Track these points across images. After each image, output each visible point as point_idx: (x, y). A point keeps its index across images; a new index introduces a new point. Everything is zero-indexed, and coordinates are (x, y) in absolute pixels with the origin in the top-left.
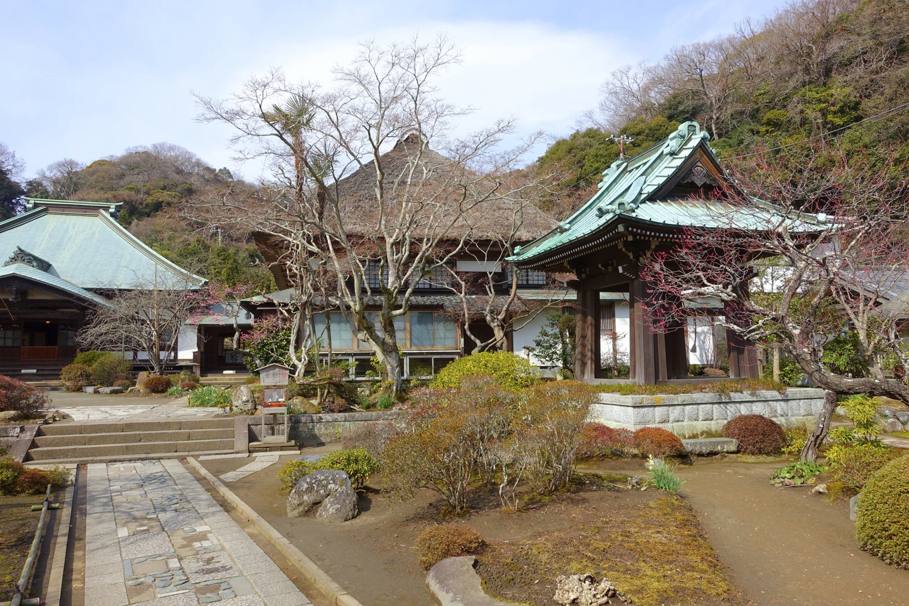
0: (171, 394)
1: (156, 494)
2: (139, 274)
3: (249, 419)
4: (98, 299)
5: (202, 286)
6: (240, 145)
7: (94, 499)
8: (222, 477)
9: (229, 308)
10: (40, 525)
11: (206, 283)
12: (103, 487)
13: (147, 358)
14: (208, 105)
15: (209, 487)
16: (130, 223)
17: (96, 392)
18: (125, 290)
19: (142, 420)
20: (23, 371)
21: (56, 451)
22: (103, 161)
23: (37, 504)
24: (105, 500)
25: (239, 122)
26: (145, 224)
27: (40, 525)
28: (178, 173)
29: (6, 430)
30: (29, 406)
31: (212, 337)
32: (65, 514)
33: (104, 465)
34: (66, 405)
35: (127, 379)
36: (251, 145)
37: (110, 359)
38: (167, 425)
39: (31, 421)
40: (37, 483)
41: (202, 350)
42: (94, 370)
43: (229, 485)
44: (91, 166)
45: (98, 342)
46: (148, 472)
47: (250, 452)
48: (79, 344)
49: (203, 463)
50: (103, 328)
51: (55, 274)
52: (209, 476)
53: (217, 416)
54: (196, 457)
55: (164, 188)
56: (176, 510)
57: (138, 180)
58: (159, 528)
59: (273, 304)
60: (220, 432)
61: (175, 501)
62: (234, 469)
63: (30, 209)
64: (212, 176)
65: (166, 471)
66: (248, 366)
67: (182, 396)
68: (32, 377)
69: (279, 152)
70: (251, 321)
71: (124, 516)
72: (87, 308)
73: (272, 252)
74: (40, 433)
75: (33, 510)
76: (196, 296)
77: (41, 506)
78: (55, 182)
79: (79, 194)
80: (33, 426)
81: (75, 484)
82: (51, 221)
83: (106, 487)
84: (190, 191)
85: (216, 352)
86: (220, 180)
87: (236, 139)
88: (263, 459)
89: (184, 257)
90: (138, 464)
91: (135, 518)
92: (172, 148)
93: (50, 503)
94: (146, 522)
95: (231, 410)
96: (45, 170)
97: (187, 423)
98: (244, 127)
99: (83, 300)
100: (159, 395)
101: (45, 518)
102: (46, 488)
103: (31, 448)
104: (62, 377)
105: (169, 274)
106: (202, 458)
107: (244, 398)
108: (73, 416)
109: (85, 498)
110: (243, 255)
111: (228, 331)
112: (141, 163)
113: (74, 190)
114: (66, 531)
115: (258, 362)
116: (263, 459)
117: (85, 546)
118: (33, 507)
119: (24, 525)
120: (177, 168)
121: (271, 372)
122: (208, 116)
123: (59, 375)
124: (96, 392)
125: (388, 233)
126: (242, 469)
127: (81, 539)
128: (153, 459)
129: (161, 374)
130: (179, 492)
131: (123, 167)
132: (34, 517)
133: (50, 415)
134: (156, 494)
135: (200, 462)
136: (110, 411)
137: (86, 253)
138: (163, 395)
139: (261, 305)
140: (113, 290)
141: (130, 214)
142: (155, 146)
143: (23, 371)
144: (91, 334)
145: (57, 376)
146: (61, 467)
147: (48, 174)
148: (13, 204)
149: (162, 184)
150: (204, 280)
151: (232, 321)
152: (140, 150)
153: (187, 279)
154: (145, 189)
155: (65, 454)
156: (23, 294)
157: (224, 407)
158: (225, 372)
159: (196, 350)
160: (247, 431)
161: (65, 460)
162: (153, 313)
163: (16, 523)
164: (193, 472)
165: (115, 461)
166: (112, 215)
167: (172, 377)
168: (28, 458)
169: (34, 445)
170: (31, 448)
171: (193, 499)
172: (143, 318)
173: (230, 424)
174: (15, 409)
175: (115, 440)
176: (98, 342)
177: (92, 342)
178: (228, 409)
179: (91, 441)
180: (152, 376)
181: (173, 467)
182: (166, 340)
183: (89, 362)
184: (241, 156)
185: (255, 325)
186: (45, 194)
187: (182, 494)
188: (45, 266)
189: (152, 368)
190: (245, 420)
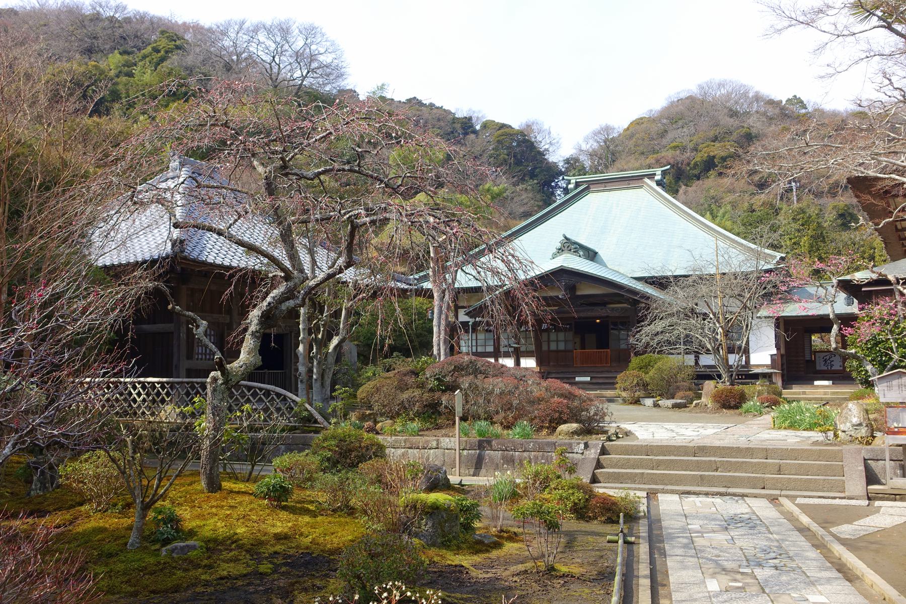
0: (747, 411)
1: (748, 542)
2: (696, 253)
3: (866, 451)
4: (650, 290)
5: (778, 263)
6: (827, 56)
7: (672, 537)
8: (834, 530)
9: (821, 291)
10: (619, 560)
11: (782, 259)
12: (680, 524)
13: (713, 363)
14: (778, 11)
15: (816, 542)
16: (677, 191)
17: (656, 405)
18: (681, 276)
19: (717, 443)
20: (577, 379)
21: (623, 474)
22: (641, 119)
23: (612, 534)
24: (685, 541)
25: (824, 22)
26: (695, 189)
27: (619, 560)
28: (731, 116)
29: (570, 445)
30: (590, 420)
31: (796, 334)
32: (643, 550)
33: (676, 497)
34: (627, 420)
35: (690, 389)
36: (843, 52)
37: (669, 365)
38: (749, 452)
39: (594, 436)
40: (609, 510)
41: (783, 351)
42: (651, 378)
43: (844, 542)
44: (628, 129)
45: (654, 343)
46: (732, 512)
47: (869, 499)
48: (633, 347)
49: (803, 508)
50: (658, 326)
51: (602, 263)
52: (814, 527)
53: (816, 443)
54: (792, 498)
55: (715, 139)
56: (776, 568)
57: (681, 135)
58: (755, 589)
59: (887, 282)
60: (818, 471)
61: (773, 555)
62: (850, 522)
63: (572, 190)
64: (777, 111)
65: (754, 513)
66: (854, 374)
67: (761, 414)
68: (586, 386)
69: (887, 52)
70: (854, 309)
71: (711, 565)
72: (638, 302)
73: (881, 204)
74: (604, 451)
75: (609, 542)
76: (772, 277)
77: (616, 538)
78: (592, 155)
79: (618, 164)
80: (597, 442)
81: (648, 515)
82: (593, 200)
83: (682, 524)
84: (749, 138)
85: (804, 354)
86: (789, 115)
87: (821, 48)
88: (891, 511)
89: (750, 225)
90: (718, 500)
91: (724, 570)
92: (721, 85)
93: (625, 536)
94: (739, 577)
95: (836, 436)
96: (581, 142)
97: (775, 451)
98: (831, 29)
99: (634, 292)
100: (732, 412)
101: (623, 552)
102: (619, 517)
103: (596, 468)
104: (617, 386)
105: (733, 252)
106: (799, 501)
107: (855, 420)
108: (637, 434)
109: (661, 535)
110: (830, 216)
111: (821, 324)
112: (685, 112)
113: (615, 160)
114: (648, 572)
115: (869, 367)
116: (891, 511)
117: (670, 594)
118: (609, 537)
119: (602, 557)
120: (731, 110)
121: (895, 382)
122: (779, 27)
123: (614, 384)
124: (656, 405)
125: (470, 312)
126: (861, 522)
127: (665, 585)
128: (734, 495)
129: (732, 384)
130: (776, 544)
131: (665, 121)
132: (610, 550)
133: (612, 431)
134: (748, 542)
135: (798, 505)
136: (676, 430)
137: (632, 235)
138: (737, 411)
139: (869, 284)
140: (667, 278)
141: (677, 180)
142: (701, 87)
143: (577, 379)
144: (647, 333)
145: (611, 385)
146: (632, 493)
147: (584, 147)
148: (552, 187)
149: (711, 134)
150: (779, 255)
151: (825, 310)
152: (683, 95)
153: (758, 256)
154: (691, 145)
155: (632, 478)
156: (572, 289)
157: (825, 432)
158: (816, 383)
159: (774, 351)
160: (862, 468)
161: (633, 486)
162: (716, 304)
163: (593, 553)
164: (790, 517)
165: (689, 493)
166: (659, 183)
167: (747, 389)
168: (594, 480)
169: (599, 465)
170: (596, 468)
171: (797, 555)
172: (705, 311)
173: (838, 456)
174: (577, 421)
175: (686, 466)
176: (654, 343)
177: (648, 344)
178: (831, 434)
179: (658, 465)
180: (720, 386)
181: (761, 508)
182: (735, 339)
183: (645, 367)
184: (831, 71)
185: (862, 314)
186: (582, 171)
187: (780, 547)
188: (591, 255)
189: (720, 376)
190: (859, 451)
